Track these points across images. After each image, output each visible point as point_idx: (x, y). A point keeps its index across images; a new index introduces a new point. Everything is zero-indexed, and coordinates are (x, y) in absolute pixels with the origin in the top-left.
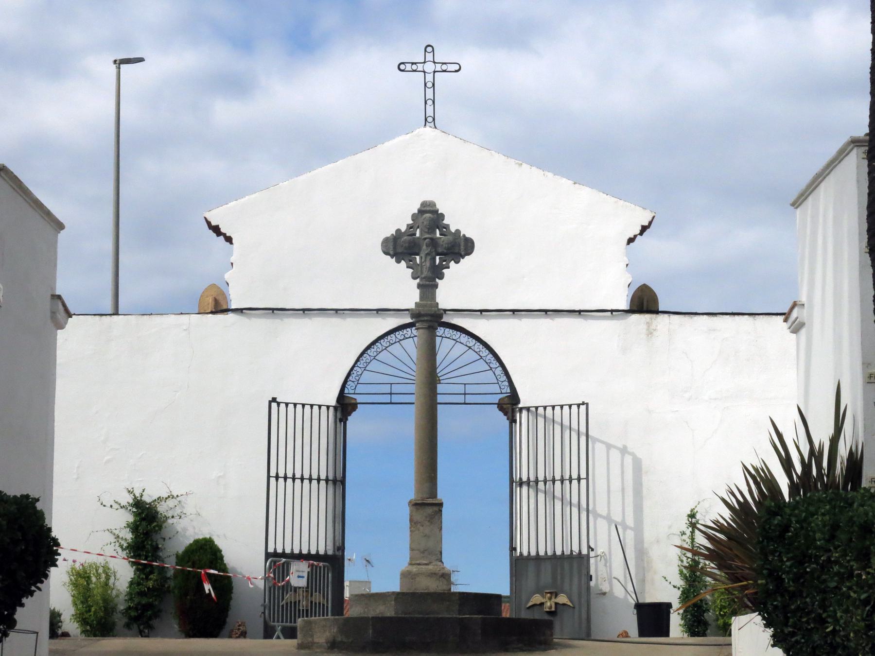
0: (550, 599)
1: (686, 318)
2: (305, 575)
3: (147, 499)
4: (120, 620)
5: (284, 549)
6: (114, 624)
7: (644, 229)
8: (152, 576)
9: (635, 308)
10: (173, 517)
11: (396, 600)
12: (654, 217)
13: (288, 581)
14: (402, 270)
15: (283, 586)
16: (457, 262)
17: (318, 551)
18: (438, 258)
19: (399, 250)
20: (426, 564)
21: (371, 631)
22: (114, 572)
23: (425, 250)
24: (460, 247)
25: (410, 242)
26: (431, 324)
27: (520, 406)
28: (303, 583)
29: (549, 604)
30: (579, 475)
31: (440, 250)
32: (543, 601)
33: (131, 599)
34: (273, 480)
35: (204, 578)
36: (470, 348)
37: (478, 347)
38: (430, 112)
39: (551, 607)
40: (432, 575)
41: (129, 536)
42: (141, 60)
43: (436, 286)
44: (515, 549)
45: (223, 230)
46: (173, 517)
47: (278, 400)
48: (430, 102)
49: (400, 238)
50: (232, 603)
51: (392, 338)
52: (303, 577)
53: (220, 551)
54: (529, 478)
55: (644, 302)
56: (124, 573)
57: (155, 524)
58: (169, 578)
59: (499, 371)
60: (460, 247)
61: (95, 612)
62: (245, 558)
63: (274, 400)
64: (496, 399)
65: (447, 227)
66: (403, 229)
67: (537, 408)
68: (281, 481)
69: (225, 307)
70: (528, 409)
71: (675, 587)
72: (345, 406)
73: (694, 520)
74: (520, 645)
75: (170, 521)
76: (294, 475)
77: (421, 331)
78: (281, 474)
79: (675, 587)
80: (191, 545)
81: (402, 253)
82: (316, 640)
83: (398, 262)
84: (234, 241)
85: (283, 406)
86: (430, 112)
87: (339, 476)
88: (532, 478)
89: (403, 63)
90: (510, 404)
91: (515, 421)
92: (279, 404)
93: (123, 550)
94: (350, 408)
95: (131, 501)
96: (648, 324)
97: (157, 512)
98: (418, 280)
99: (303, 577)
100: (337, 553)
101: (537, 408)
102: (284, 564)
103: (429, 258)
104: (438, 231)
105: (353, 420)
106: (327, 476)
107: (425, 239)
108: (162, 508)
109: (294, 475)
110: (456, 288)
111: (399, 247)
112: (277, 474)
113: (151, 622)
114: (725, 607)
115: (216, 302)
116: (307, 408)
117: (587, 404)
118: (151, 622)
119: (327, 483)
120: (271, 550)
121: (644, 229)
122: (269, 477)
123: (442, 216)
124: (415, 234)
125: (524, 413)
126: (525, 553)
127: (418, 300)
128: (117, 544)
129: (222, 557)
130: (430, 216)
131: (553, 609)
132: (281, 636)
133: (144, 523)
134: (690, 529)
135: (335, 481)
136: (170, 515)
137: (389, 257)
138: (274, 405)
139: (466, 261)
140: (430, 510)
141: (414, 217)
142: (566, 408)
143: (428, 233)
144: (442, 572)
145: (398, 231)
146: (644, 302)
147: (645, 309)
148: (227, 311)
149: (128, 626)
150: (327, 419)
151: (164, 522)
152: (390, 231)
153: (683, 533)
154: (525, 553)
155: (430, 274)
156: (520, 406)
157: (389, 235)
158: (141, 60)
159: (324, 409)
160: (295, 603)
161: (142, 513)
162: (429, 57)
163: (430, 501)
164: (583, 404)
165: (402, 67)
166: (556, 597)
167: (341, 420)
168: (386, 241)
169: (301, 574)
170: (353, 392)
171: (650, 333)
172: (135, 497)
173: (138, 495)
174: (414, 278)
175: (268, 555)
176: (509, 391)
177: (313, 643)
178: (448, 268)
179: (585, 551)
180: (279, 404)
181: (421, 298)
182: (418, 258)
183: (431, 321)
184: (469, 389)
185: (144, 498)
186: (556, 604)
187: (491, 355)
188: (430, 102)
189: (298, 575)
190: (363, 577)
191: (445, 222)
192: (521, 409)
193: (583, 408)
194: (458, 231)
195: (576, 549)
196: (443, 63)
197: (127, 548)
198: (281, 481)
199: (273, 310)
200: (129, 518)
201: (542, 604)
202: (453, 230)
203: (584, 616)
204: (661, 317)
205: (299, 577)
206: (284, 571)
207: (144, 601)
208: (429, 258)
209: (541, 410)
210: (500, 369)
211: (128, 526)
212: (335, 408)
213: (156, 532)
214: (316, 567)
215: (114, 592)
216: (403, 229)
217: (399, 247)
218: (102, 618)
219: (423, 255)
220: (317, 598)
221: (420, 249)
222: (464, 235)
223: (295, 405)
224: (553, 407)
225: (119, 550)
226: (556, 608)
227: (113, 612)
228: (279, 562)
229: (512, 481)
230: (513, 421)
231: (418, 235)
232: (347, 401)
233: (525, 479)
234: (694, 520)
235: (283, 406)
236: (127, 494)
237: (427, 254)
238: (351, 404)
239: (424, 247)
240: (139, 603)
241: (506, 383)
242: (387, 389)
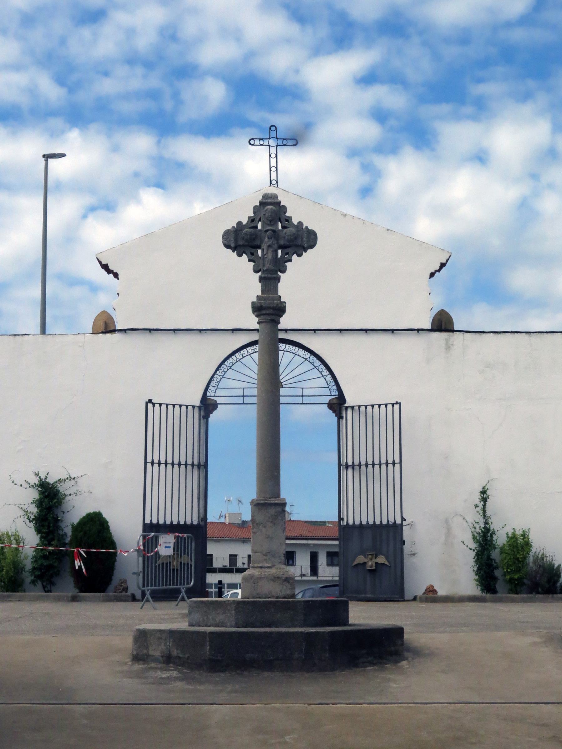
0: (371, 559)
1: (477, 335)
2: (172, 545)
3: (51, 480)
4: (28, 578)
5: (158, 521)
6: (23, 581)
7: (443, 265)
8: (53, 543)
9: (435, 328)
10: (70, 495)
11: (236, 608)
12: (450, 256)
13: (157, 553)
14: (243, 265)
15: (152, 556)
16: (299, 255)
17: (185, 521)
18: (280, 251)
19: (241, 243)
20: (269, 567)
21: (208, 648)
22: (23, 539)
23: (266, 242)
24: (301, 240)
25: (251, 234)
26: (273, 317)
27: (346, 405)
28: (170, 552)
29: (370, 564)
30: (394, 460)
31: (282, 242)
32: (366, 560)
33: (36, 561)
34: (149, 465)
35: (76, 555)
36: (306, 359)
37: (312, 358)
38: (274, 177)
39: (371, 566)
40: (275, 579)
41: (34, 510)
42: (63, 155)
43: (278, 279)
44: (343, 519)
45: (111, 268)
46: (70, 495)
47: (153, 401)
48: (274, 169)
49: (242, 230)
50: (116, 564)
51: (244, 352)
52: (170, 547)
53: (107, 522)
54: (353, 462)
55: (442, 324)
56: (31, 539)
57: (56, 500)
58: (67, 544)
59: (329, 378)
60: (301, 240)
61: (7, 572)
62: (127, 529)
63: (150, 401)
64: (327, 400)
65: (288, 220)
66: (245, 222)
67: (359, 407)
68: (156, 466)
69: (112, 328)
70: (352, 407)
71: (471, 549)
72: (207, 406)
73: (485, 496)
74: (370, 659)
75: (68, 498)
76: (166, 461)
77: (263, 325)
78: (156, 461)
79: (471, 549)
80: (84, 517)
81: (243, 246)
82: (151, 652)
83: (240, 255)
84: (119, 276)
85: (157, 406)
86: (274, 177)
87: (202, 462)
88: (356, 462)
89: (253, 139)
90: (338, 405)
91: (342, 417)
92: (154, 404)
93: (30, 521)
94: (211, 408)
95: (37, 482)
96: (447, 340)
97: (58, 491)
98: (260, 274)
99: (170, 547)
100: (201, 523)
101: (359, 407)
102: (153, 537)
103: (270, 250)
104: (279, 223)
105: (214, 417)
106: (193, 462)
107: (267, 231)
108: (62, 488)
109: (166, 461)
110: (297, 280)
111: (241, 240)
112: (153, 460)
113: (53, 580)
114: (511, 566)
115: (106, 324)
116: (177, 407)
117: (400, 404)
118: (53, 580)
119: (193, 468)
120: (148, 521)
121: (443, 265)
122: (146, 463)
123: (284, 209)
124: (256, 227)
125: (350, 411)
126: (351, 523)
127: (259, 293)
128: (26, 517)
129: (108, 527)
130: (271, 209)
131: (374, 568)
132: (150, 599)
133: (46, 500)
134: (482, 503)
135: (199, 466)
136: (69, 493)
137: (230, 251)
138: (150, 405)
139: (309, 255)
140: (272, 511)
141: (256, 210)
142: (383, 407)
143: (270, 225)
144: (286, 575)
145: (239, 223)
146: (442, 324)
147: (443, 327)
148: (113, 331)
149: (33, 582)
150: (195, 417)
151: (64, 499)
152: (231, 224)
153: (477, 506)
154: (351, 523)
155: (272, 268)
156: (346, 405)
157: (229, 227)
158: (63, 155)
159: (190, 408)
160: (167, 564)
161: (46, 492)
162: (273, 134)
163: (273, 501)
164: (397, 403)
165: (252, 142)
166: (376, 558)
167: (204, 417)
168: (227, 234)
169: (168, 545)
170: (213, 394)
171: (448, 347)
172: (41, 479)
173: (42, 477)
174: (256, 271)
175: (145, 525)
176: (337, 393)
177: (148, 656)
178: (290, 261)
179: (398, 521)
180: (154, 404)
181: (263, 291)
182: (259, 251)
183: (272, 314)
184: (306, 392)
185: (48, 480)
186: (376, 563)
187: (322, 366)
188: (274, 169)
189: (166, 546)
190: (236, 511)
191: (287, 214)
192: (347, 408)
193: (396, 407)
194: (300, 224)
195: (392, 520)
196: (284, 139)
197: (33, 519)
198: (156, 466)
199: (150, 330)
200: (35, 495)
201: (365, 563)
202: (295, 222)
203: (399, 573)
204: (456, 335)
205: (166, 547)
206: (155, 542)
207: (46, 563)
208: (270, 250)
209: (363, 408)
210: (330, 376)
211: (34, 502)
212: (200, 408)
213: (57, 507)
214: (181, 538)
215: (23, 555)
216: (245, 222)
217: (241, 240)
218: (12, 577)
219: (264, 246)
220: (185, 559)
221: (262, 242)
222: (307, 228)
223: (167, 405)
224: (373, 406)
225: (27, 521)
226: (376, 566)
227: (22, 570)
228: (152, 530)
229: (340, 465)
230: (340, 417)
231: (259, 227)
232: (209, 402)
233: (350, 463)
234: (485, 496)
235: (157, 406)
236: (34, 476)
237: (269, 246)
238: (212, 404)
239: (266, 239)
240: (42, 565)
241: (335, 387)
242: (240, 392)
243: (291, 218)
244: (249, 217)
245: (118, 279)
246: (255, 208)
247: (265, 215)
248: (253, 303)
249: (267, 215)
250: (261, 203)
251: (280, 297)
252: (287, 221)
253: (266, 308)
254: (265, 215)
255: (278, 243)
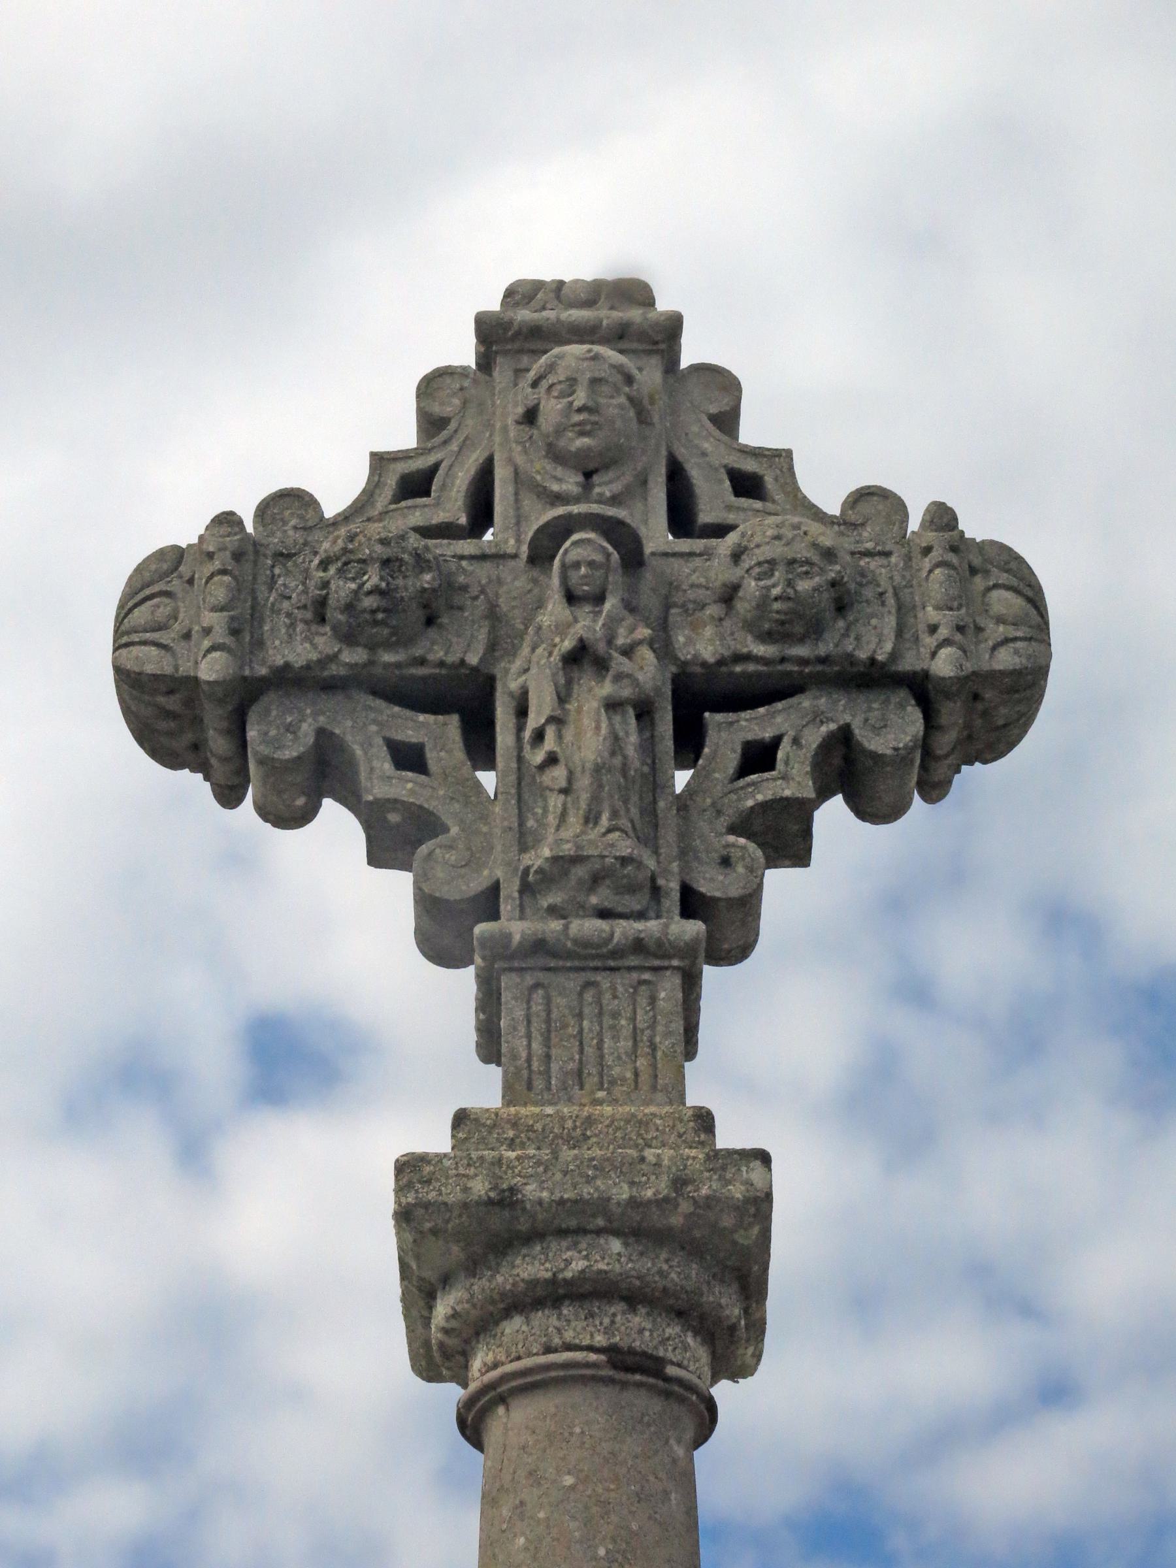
14: (332, 907)
60: (882, 670)
66: (336, 492)
183: (633, 1297)
202: (826, 489)
243: (782, 458)
244: (380, 461)
245: (482, 1450)
246: (433, 384)
247: (530, 416)
248: (410, 1169)
249: (551, 410)
250: (492, 334)
251: (962, 532)
252: (746, 485)
253: (574, 1222)
254: (530, 416)
255: (663, 647)
